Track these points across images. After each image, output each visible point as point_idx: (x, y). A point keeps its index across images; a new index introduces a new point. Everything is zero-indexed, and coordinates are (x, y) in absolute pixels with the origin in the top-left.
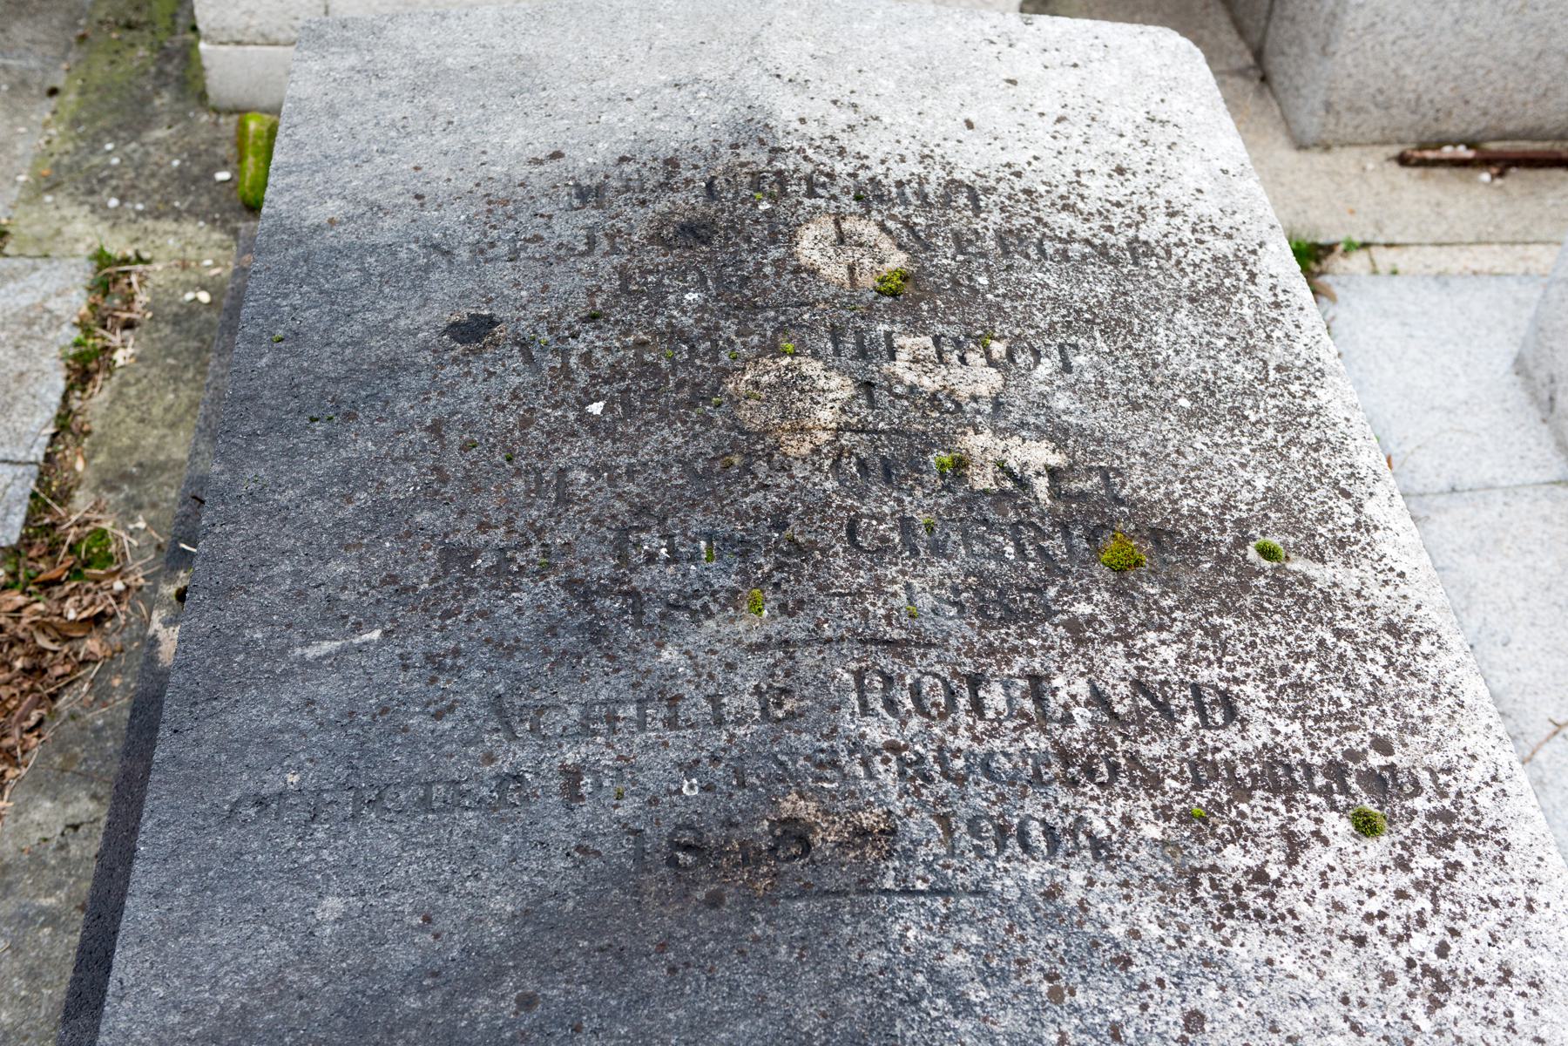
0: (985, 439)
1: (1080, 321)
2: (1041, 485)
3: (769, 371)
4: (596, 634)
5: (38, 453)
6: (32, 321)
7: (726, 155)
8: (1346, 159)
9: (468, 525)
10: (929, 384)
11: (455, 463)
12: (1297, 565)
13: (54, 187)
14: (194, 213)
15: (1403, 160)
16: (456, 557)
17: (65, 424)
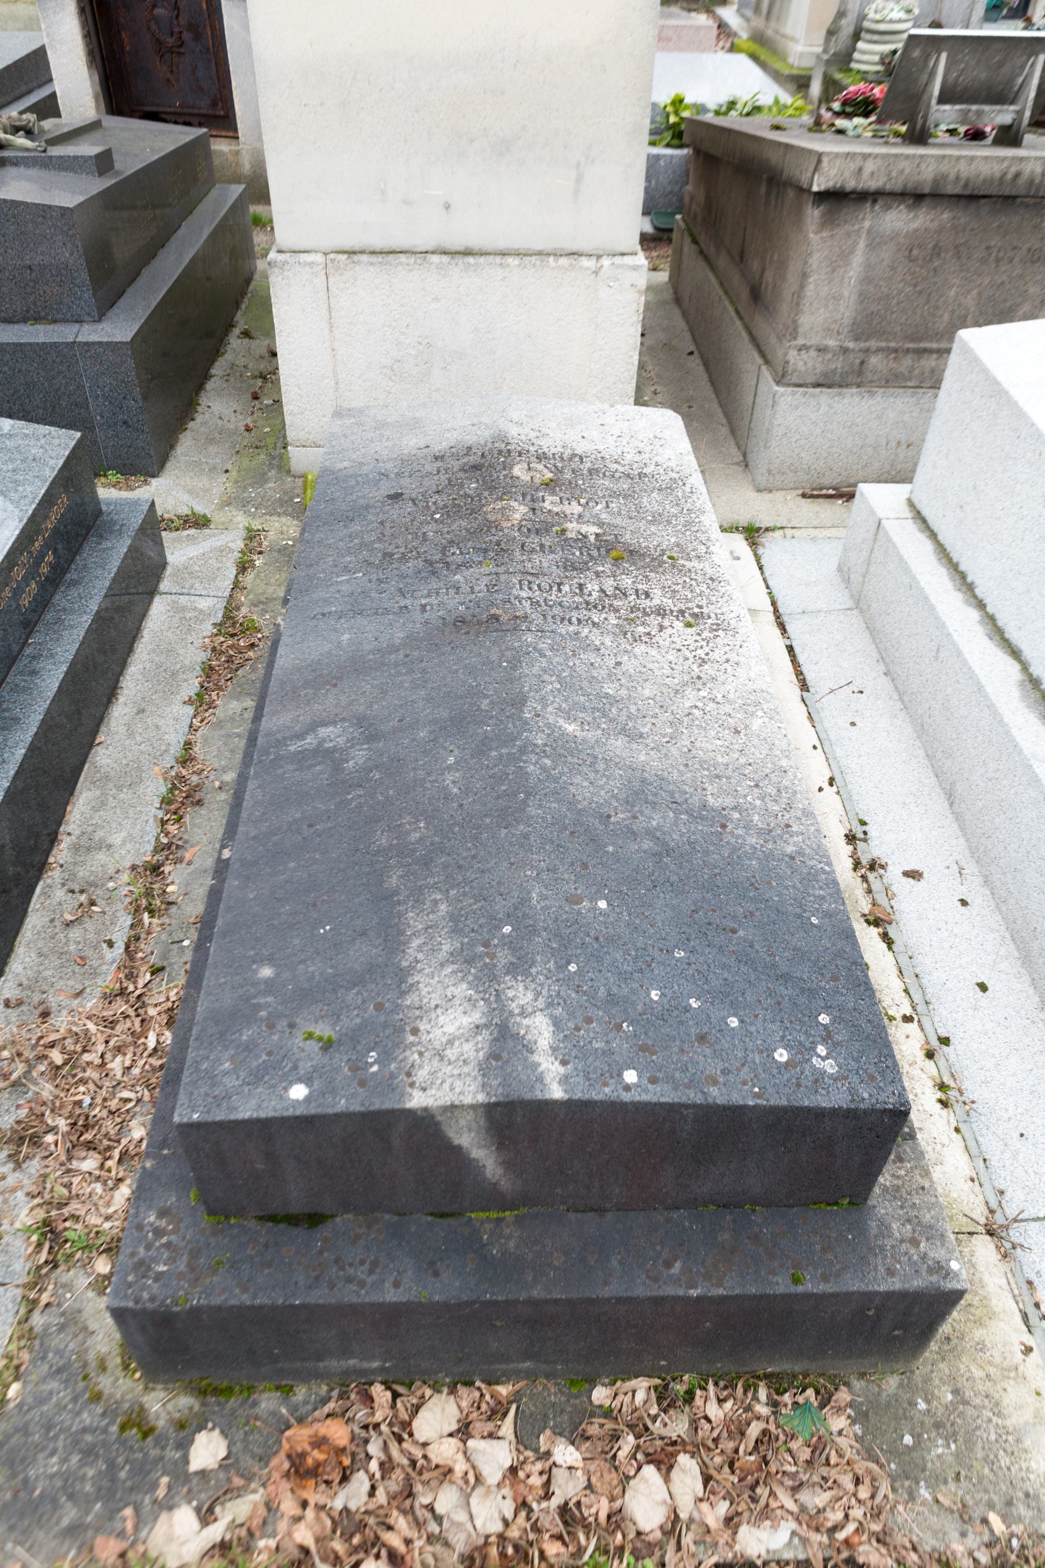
0: (574, 524)
1: (615, 495)
2: (592, 538)
3: (499, 505)
4: (434, 573)
5: (227, 594)
6: (222, 551)
7: (489, 445)
8: (779, 496)
9: (392, 547)
10: (555, 509)
11: (388, 532)
12: (681, 562)
13: (229, 504)
14: (285, 514)
15: (804, 496)
16: (387, 555)
17: (236, 585)
